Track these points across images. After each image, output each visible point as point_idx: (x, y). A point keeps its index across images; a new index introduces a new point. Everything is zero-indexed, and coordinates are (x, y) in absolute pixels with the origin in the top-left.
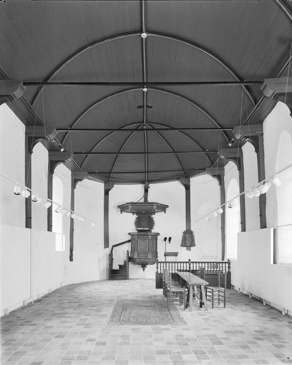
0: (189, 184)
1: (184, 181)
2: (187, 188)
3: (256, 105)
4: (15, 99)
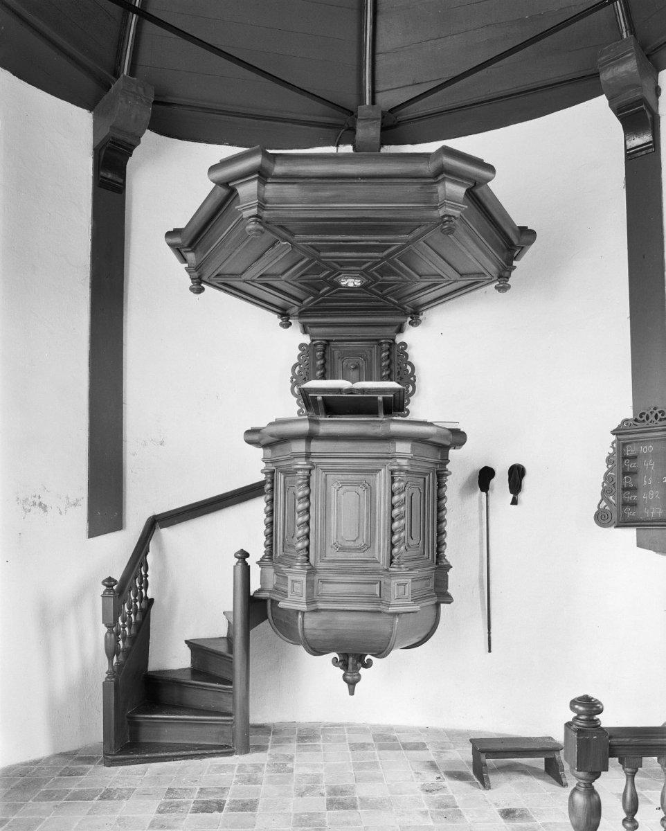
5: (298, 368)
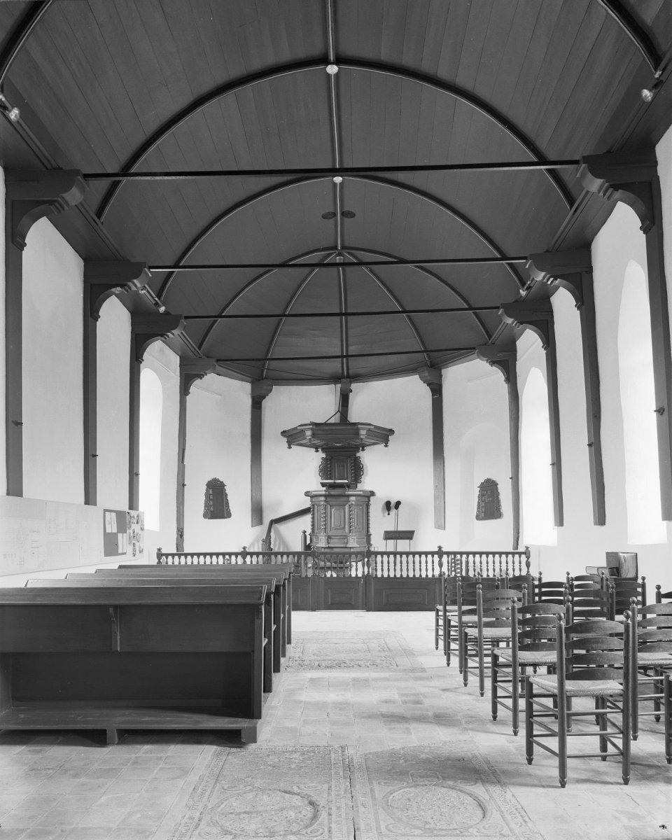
2: (437, 390)
3: (571, 208)
4: (66, 208)
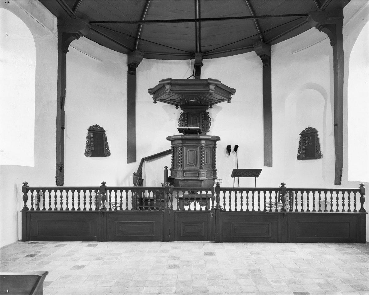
0: (269, 56)
1: (261, 47)
5: (180, 119)
